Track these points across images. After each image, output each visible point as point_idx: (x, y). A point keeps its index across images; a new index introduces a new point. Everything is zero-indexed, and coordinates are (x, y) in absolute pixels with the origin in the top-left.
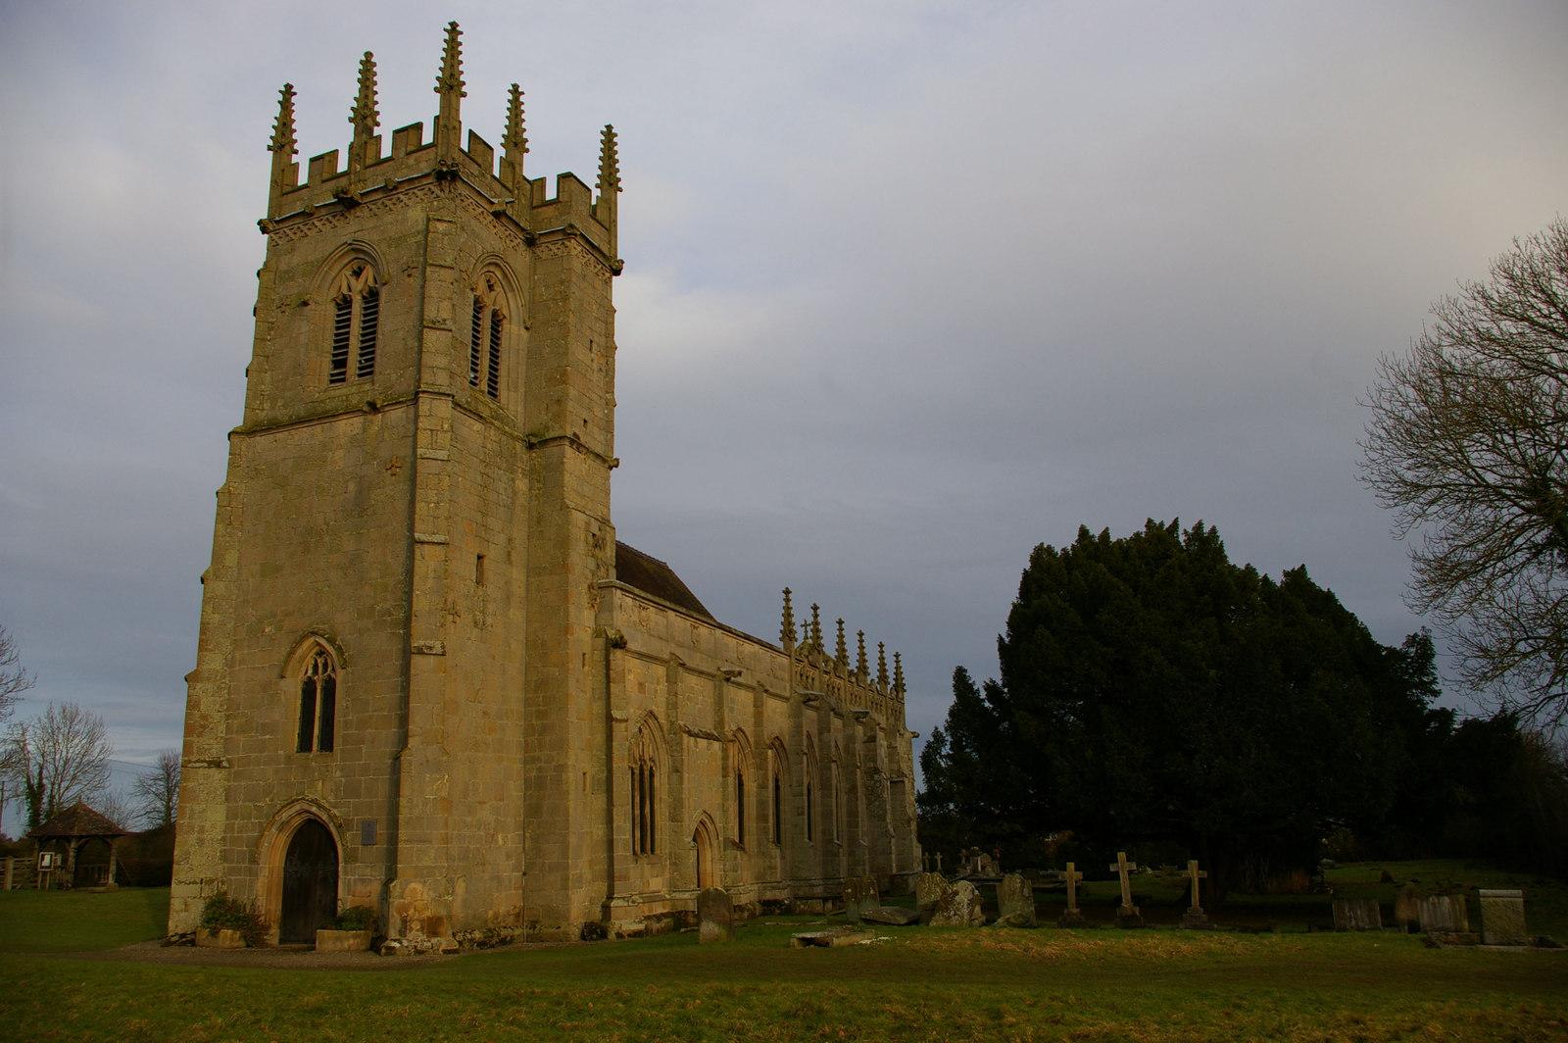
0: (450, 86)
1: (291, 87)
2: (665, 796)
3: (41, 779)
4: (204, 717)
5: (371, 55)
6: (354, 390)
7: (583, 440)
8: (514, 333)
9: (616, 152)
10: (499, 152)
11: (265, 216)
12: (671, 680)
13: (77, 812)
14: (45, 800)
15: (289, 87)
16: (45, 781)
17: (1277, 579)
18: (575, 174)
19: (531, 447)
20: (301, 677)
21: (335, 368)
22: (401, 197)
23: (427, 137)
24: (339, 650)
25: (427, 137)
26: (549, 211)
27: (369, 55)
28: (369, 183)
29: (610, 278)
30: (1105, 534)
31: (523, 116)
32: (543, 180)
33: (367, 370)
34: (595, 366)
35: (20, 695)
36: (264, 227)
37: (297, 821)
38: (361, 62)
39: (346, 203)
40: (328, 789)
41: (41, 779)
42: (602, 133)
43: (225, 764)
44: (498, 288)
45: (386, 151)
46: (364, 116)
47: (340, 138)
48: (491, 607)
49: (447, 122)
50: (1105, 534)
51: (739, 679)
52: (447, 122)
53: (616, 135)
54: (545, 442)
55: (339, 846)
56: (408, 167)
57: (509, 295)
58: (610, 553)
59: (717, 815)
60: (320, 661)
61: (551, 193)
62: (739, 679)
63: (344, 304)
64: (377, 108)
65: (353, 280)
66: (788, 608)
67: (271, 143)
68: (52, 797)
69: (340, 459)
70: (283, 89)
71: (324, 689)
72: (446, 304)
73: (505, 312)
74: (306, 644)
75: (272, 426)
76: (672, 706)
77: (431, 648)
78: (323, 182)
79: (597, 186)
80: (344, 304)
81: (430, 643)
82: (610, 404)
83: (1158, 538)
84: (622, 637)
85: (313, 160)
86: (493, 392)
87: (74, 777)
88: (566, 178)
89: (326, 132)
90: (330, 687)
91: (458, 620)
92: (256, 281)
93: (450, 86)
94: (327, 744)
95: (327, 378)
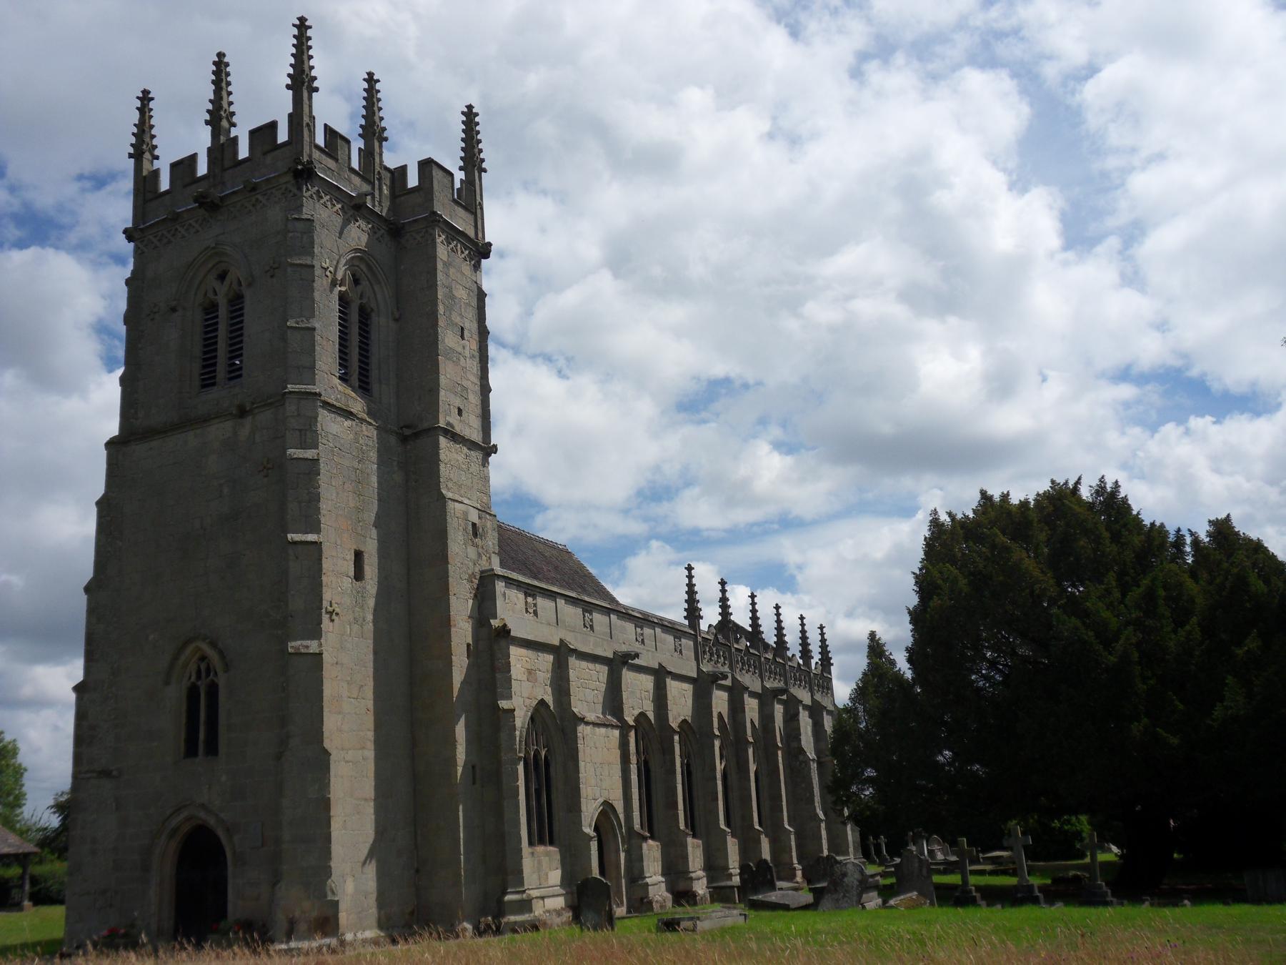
0: (302, 82)
1: (149, 92)
5: (224, 55)
6: (220, 395)
9: (478, 132)
10: (357, 144)
11: (130, 225)
15: (146, 92)
17: (1203, 533)
19: (404, 439)
22: (260, 197)
23: (283, 136)
24: (221, 654)
33: (235, 373)
37: (186, 828)
42: (463, 113)
43: (115, 773)
44: (365, 283)
47: (199, 141)
49: (300, 119)
50: (1005, 497)
51: (636, 661)
52: (300, 119)
53: (477, 115)
54: (417, 435)
57: (376, 288)
58: (491, 541)
59: (619, 807)
60: (203, 667)
61: (413, 180)
62: (636, 661)
63: (211, 309)
65: (217, 284)
66: (691, 586)
67: (132, 151)
70: (297, 22)
73: (373, 305)
74: (190, 648)
78: (185, 186)
79: (461, 169)
80: (211, 309)
83: (1061, 499)
84: (505, 625)
85: (252, 133)
90: (213, 691)
93: (302, 82)
94: (212, 749)
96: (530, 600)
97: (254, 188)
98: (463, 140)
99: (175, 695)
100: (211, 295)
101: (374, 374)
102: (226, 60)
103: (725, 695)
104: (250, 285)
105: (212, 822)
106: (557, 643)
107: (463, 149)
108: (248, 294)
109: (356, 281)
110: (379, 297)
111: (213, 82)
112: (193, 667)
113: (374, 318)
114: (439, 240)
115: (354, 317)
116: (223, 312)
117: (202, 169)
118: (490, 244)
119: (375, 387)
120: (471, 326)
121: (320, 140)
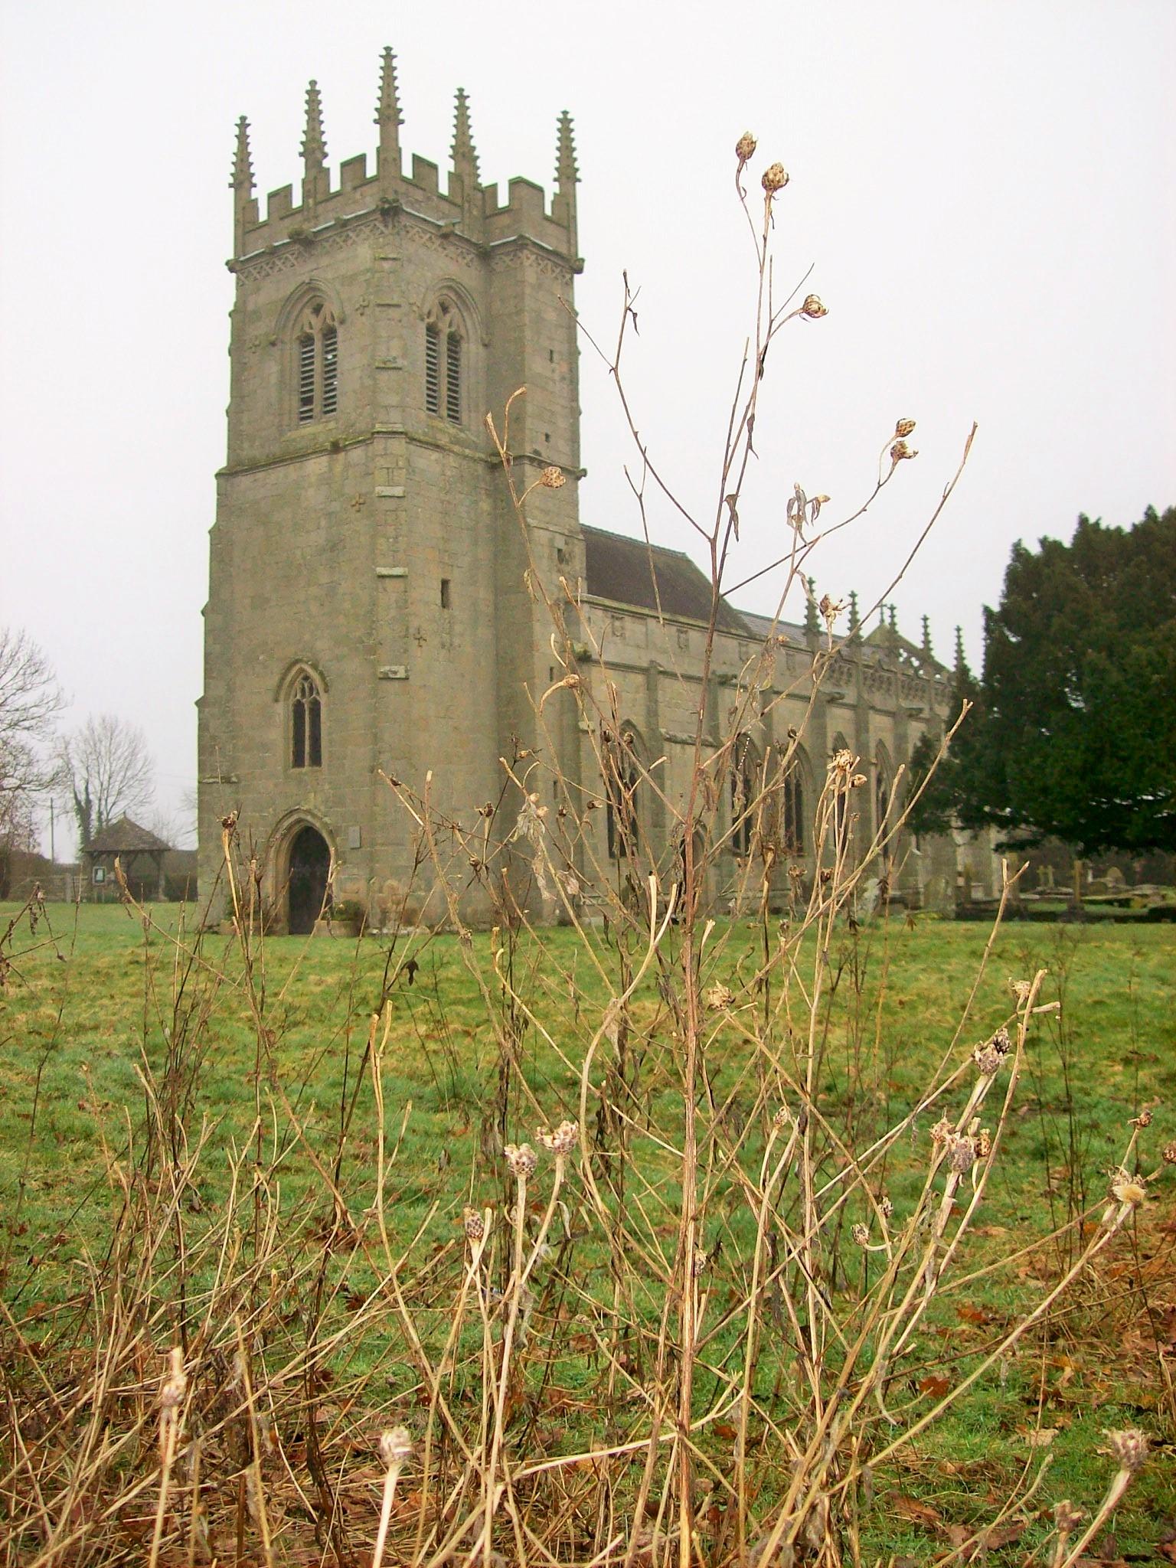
0: (389, 117)
2: (647, 803)
3: (87, 794)
4: (213, 738)
6: (317, 430)
7: (544, 457)
8: (472, 352)
12: (651, 688)
13: (125, 827)
14: (94, 816)
16: (91, 797)
18: (526, 177)
20: (292, 701)
21: (305, 405)
23: (371, 170)
24: (321, 674)
25: (371, 170)
26: (505, 220)
27: (313, 83)
28: (321, 219)
29: (572, 279)
30: (1097, 524)
31: (470, 122)
32: (494, 187)
33: (330, 406)
34: (557, 376)
35: (61, 713)
36: (232, 266)
37: (297, 829)
38: (307, 92)
39: (304, 242)
40: (315, 800)
41: (87, 794)
44: (454, 311)
45: (335, 186)
46: (313, 149)
48: (458, 628)
49: (389, 151)
50: (1097, 524)
52: (389, 151)
55: (1033, 991)
56: (355, 202)
58: (579, 564)
61: (503, 201)
64: (324, 139)
65: (314, 320)
68: (100, 813)
69: (314, 497)
71: (312, 710)
72: (395, 343)
73: (463, 332)
74: (297, 667)
75: (253, 467)
76: (652, 713)
77: (395, 673)
81: (394, 668)
82: (575, 412)
85: (344, 165)
86: (454, 417)
87: (119, 793)
88: (516, 183)
89: (279, 168)
90: (316, 707)
91: (422, 643)
92: (229, 320)
93: (389, 117)
94: (316, 760)
95: (295, 417)
96: (617, 623)
97: (345, 224)
98: (558, 149)
99: (282, 712)
100: (329, 321)
101: (463, 403)
102: (317, 88)
103: (847, 714)
104: (342, 322)
105: (318, 825)
106: (645, 665)
107: (558, 159)
108: (340, 331)
109: (445, 309)
110: (469, 323)
111: (307, 112)
112: (297, 685)
113: (464, 346)
114: (527, 263)
115: (443, 347)
116: (318, 346)
117: (297, 201)
118: (583, 260)
119: (464, 416)
120: (559, 347)
121: (407, 171)
